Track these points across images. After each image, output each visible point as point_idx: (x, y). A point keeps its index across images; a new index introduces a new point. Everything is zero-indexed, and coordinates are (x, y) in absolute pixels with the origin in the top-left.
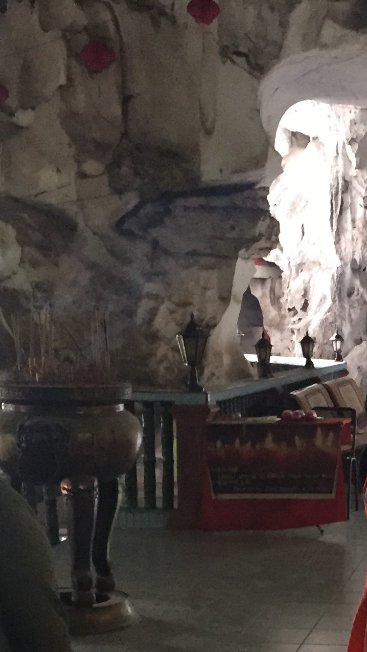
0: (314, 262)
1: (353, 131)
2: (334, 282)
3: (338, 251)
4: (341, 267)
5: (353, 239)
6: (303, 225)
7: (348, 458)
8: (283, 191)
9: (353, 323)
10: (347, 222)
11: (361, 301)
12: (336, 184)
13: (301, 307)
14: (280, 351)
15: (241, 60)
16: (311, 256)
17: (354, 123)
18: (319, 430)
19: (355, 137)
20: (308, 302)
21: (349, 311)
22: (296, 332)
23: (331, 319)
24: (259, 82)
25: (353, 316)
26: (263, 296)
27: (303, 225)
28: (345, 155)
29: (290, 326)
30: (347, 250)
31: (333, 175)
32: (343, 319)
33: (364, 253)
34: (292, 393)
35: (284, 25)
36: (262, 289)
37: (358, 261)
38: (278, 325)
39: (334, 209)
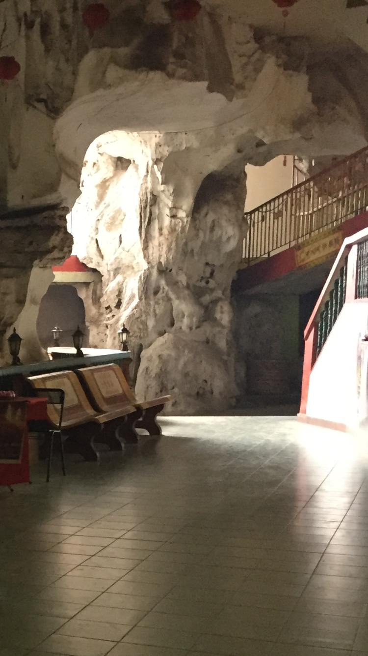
0: (128, 266)
1: (158, 152)
2: (141, 283)
3: (146, 257)
4: (148, 269)
5: (159, 245)
6: (121, 236)
7: (50, 431)
8: (105, 208)
9: (157, 317)
10: (154, 230)
11: (166, 299)
12: (145, 199)
13: (115, 306)
14: (96, 344)
15: (41, 106)
16: (126, 261)
17: (159, 145)
18: (10, 407)
19: (159, 157)
20: (122, 301)
21: (154, 307)
22: (109, 327)
23: (137, 315)
24: (55, 122)
25: (157, 312)
26: (87, 297)
27: (121, 236)
28: (153, 173)
29: (105, 322)
30: (154, 255)
31: (142, 190)
32: (147, 314)
33: (168, 256)
34: (29, 378)
35: (75, 73)
36: (87, 291)
37: (163, 263)
38: (96, 321)
39: (143, 220)
